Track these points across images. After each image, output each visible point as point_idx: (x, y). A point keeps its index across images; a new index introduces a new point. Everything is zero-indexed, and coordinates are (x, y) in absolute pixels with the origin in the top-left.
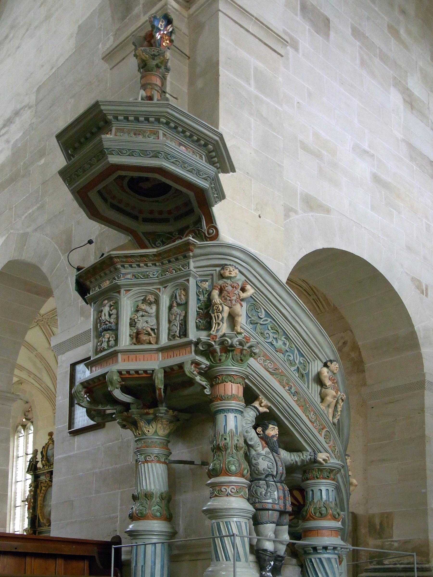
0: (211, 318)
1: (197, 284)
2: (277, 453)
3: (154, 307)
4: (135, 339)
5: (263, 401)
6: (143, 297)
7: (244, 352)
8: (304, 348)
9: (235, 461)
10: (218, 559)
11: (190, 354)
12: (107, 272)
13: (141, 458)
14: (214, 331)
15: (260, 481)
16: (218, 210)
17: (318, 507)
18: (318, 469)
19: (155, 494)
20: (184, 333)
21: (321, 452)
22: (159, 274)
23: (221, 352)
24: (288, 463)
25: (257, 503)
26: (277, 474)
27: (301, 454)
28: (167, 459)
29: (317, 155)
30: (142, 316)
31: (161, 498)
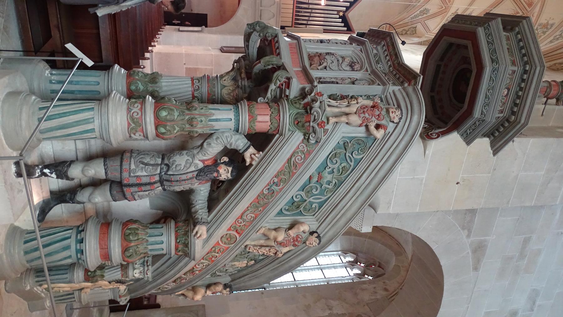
16: (455, 137)
19: (156, 85)
21: (207, 232)
26: (170, 175)
29: (522, 256)
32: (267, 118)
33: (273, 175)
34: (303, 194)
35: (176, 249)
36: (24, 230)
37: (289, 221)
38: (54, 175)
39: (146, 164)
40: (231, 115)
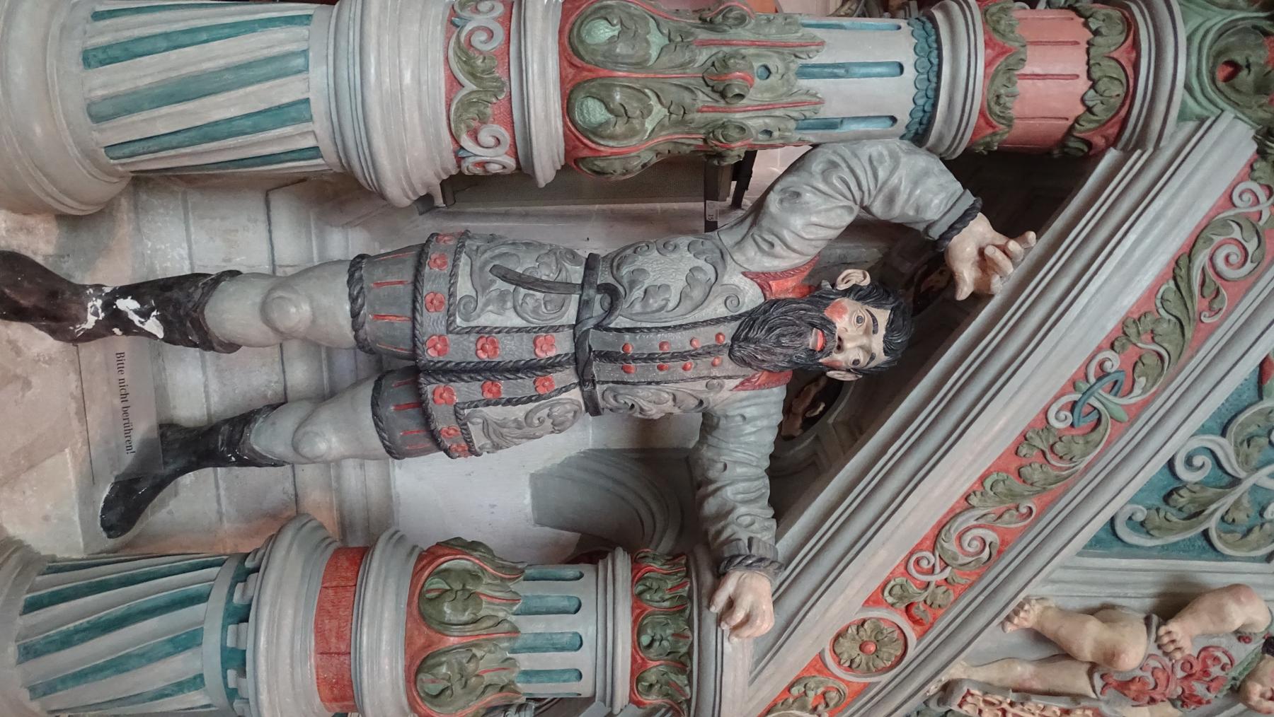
17: (481, 589)
18: (690, 597)
32: (1074, 62)
33: (1099, 337)
34: (1225, 448)
35: (637, 676)
36: (41, 558)
37: (1150, 578)
38: (153, 326)
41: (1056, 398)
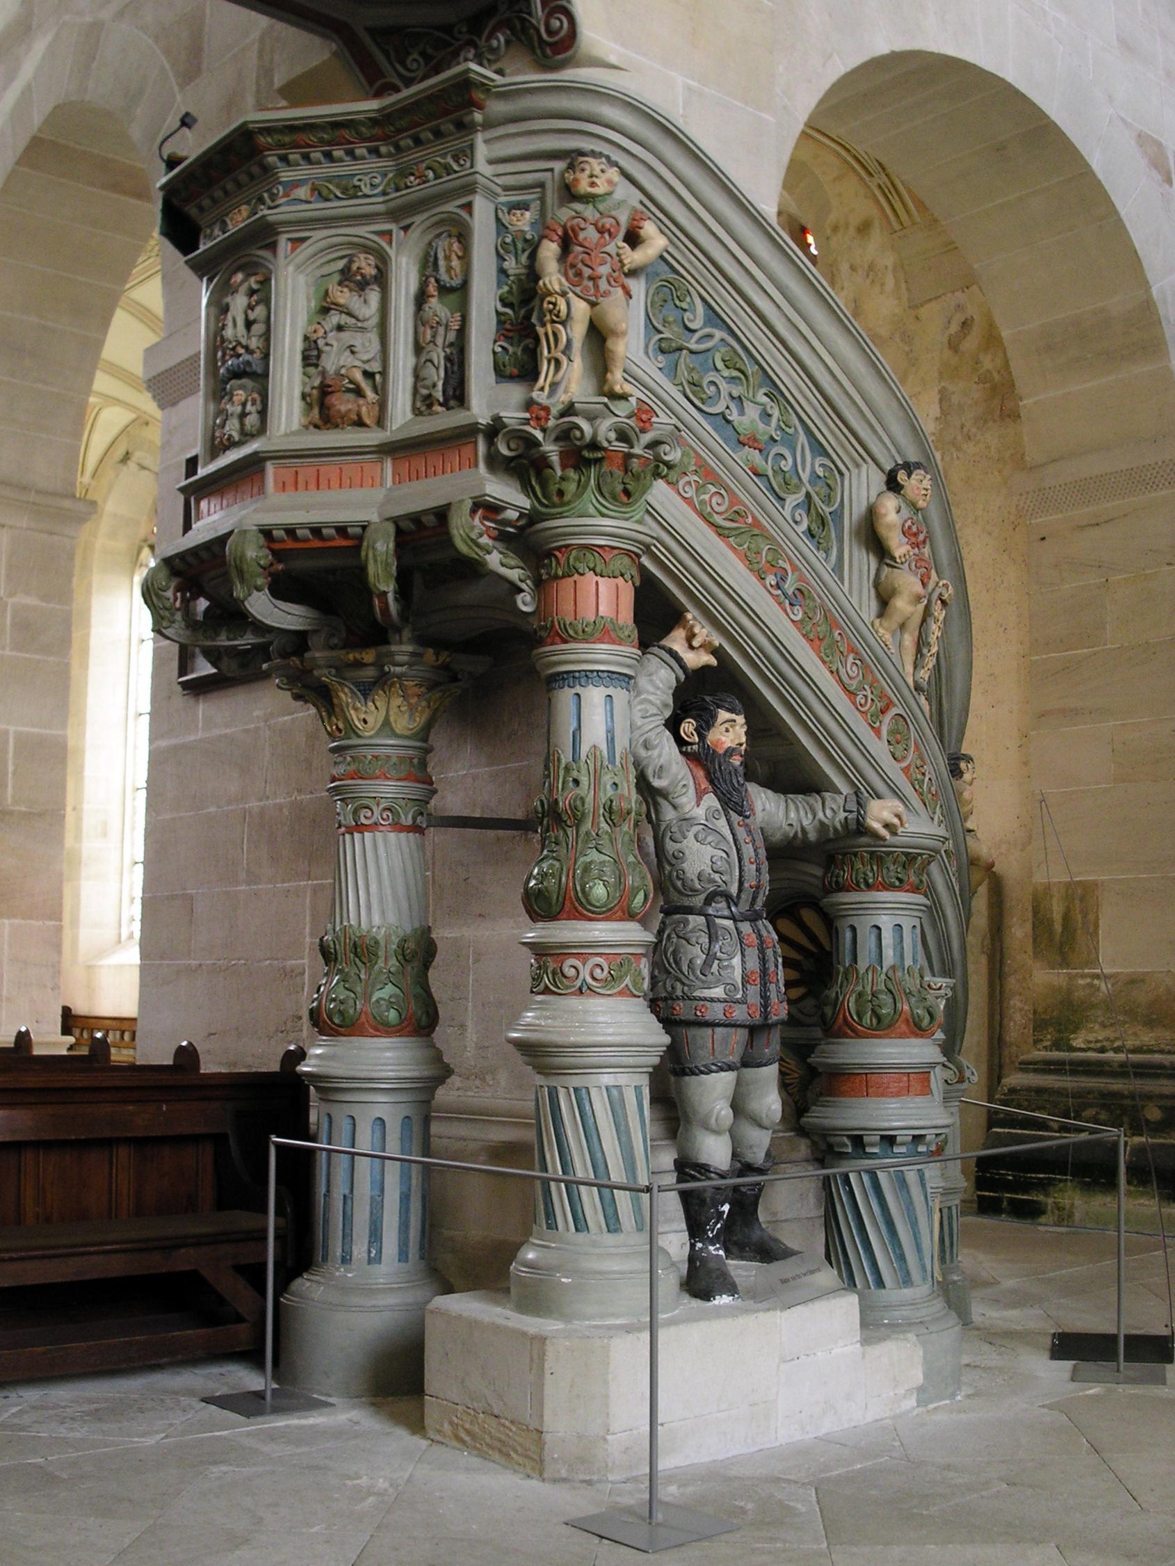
0: (537, 340)
1: (498, 219)
2: (740, 814)
3: (374, 296)
4: (316, 411)
5: (696, 630)
6: (344, 261)
7: (635, 464)
8: (826, 424)
9: (605, 863)
10: (552, 1225)
11: (473, 470)
12: (243, 178)
13: (345, 813)
14: (542, 389)
15: (691, 917)
17: (868, 989)
18: (872, 853)
19: (382, 943)
20: (457, 394)
21: (879, 797)
22: (388, 184)
23: (564, 467)
24: (777, 837)
25: (678, 998)
26: (740, 890)
27: (815, 800)
28: (421, 814)
30: (340, 328)
31: (400, 957)
39: (710, 957)
40: (594, 696)
41: (785, 611)
